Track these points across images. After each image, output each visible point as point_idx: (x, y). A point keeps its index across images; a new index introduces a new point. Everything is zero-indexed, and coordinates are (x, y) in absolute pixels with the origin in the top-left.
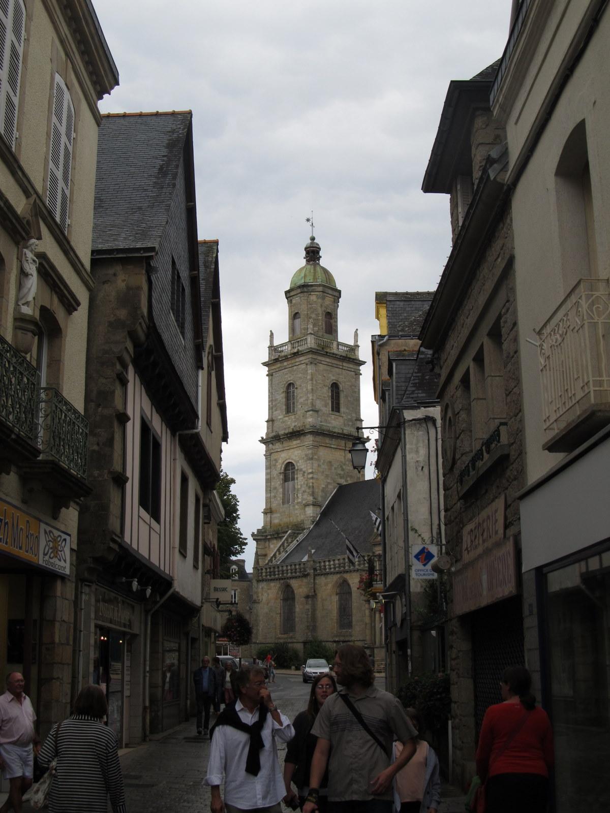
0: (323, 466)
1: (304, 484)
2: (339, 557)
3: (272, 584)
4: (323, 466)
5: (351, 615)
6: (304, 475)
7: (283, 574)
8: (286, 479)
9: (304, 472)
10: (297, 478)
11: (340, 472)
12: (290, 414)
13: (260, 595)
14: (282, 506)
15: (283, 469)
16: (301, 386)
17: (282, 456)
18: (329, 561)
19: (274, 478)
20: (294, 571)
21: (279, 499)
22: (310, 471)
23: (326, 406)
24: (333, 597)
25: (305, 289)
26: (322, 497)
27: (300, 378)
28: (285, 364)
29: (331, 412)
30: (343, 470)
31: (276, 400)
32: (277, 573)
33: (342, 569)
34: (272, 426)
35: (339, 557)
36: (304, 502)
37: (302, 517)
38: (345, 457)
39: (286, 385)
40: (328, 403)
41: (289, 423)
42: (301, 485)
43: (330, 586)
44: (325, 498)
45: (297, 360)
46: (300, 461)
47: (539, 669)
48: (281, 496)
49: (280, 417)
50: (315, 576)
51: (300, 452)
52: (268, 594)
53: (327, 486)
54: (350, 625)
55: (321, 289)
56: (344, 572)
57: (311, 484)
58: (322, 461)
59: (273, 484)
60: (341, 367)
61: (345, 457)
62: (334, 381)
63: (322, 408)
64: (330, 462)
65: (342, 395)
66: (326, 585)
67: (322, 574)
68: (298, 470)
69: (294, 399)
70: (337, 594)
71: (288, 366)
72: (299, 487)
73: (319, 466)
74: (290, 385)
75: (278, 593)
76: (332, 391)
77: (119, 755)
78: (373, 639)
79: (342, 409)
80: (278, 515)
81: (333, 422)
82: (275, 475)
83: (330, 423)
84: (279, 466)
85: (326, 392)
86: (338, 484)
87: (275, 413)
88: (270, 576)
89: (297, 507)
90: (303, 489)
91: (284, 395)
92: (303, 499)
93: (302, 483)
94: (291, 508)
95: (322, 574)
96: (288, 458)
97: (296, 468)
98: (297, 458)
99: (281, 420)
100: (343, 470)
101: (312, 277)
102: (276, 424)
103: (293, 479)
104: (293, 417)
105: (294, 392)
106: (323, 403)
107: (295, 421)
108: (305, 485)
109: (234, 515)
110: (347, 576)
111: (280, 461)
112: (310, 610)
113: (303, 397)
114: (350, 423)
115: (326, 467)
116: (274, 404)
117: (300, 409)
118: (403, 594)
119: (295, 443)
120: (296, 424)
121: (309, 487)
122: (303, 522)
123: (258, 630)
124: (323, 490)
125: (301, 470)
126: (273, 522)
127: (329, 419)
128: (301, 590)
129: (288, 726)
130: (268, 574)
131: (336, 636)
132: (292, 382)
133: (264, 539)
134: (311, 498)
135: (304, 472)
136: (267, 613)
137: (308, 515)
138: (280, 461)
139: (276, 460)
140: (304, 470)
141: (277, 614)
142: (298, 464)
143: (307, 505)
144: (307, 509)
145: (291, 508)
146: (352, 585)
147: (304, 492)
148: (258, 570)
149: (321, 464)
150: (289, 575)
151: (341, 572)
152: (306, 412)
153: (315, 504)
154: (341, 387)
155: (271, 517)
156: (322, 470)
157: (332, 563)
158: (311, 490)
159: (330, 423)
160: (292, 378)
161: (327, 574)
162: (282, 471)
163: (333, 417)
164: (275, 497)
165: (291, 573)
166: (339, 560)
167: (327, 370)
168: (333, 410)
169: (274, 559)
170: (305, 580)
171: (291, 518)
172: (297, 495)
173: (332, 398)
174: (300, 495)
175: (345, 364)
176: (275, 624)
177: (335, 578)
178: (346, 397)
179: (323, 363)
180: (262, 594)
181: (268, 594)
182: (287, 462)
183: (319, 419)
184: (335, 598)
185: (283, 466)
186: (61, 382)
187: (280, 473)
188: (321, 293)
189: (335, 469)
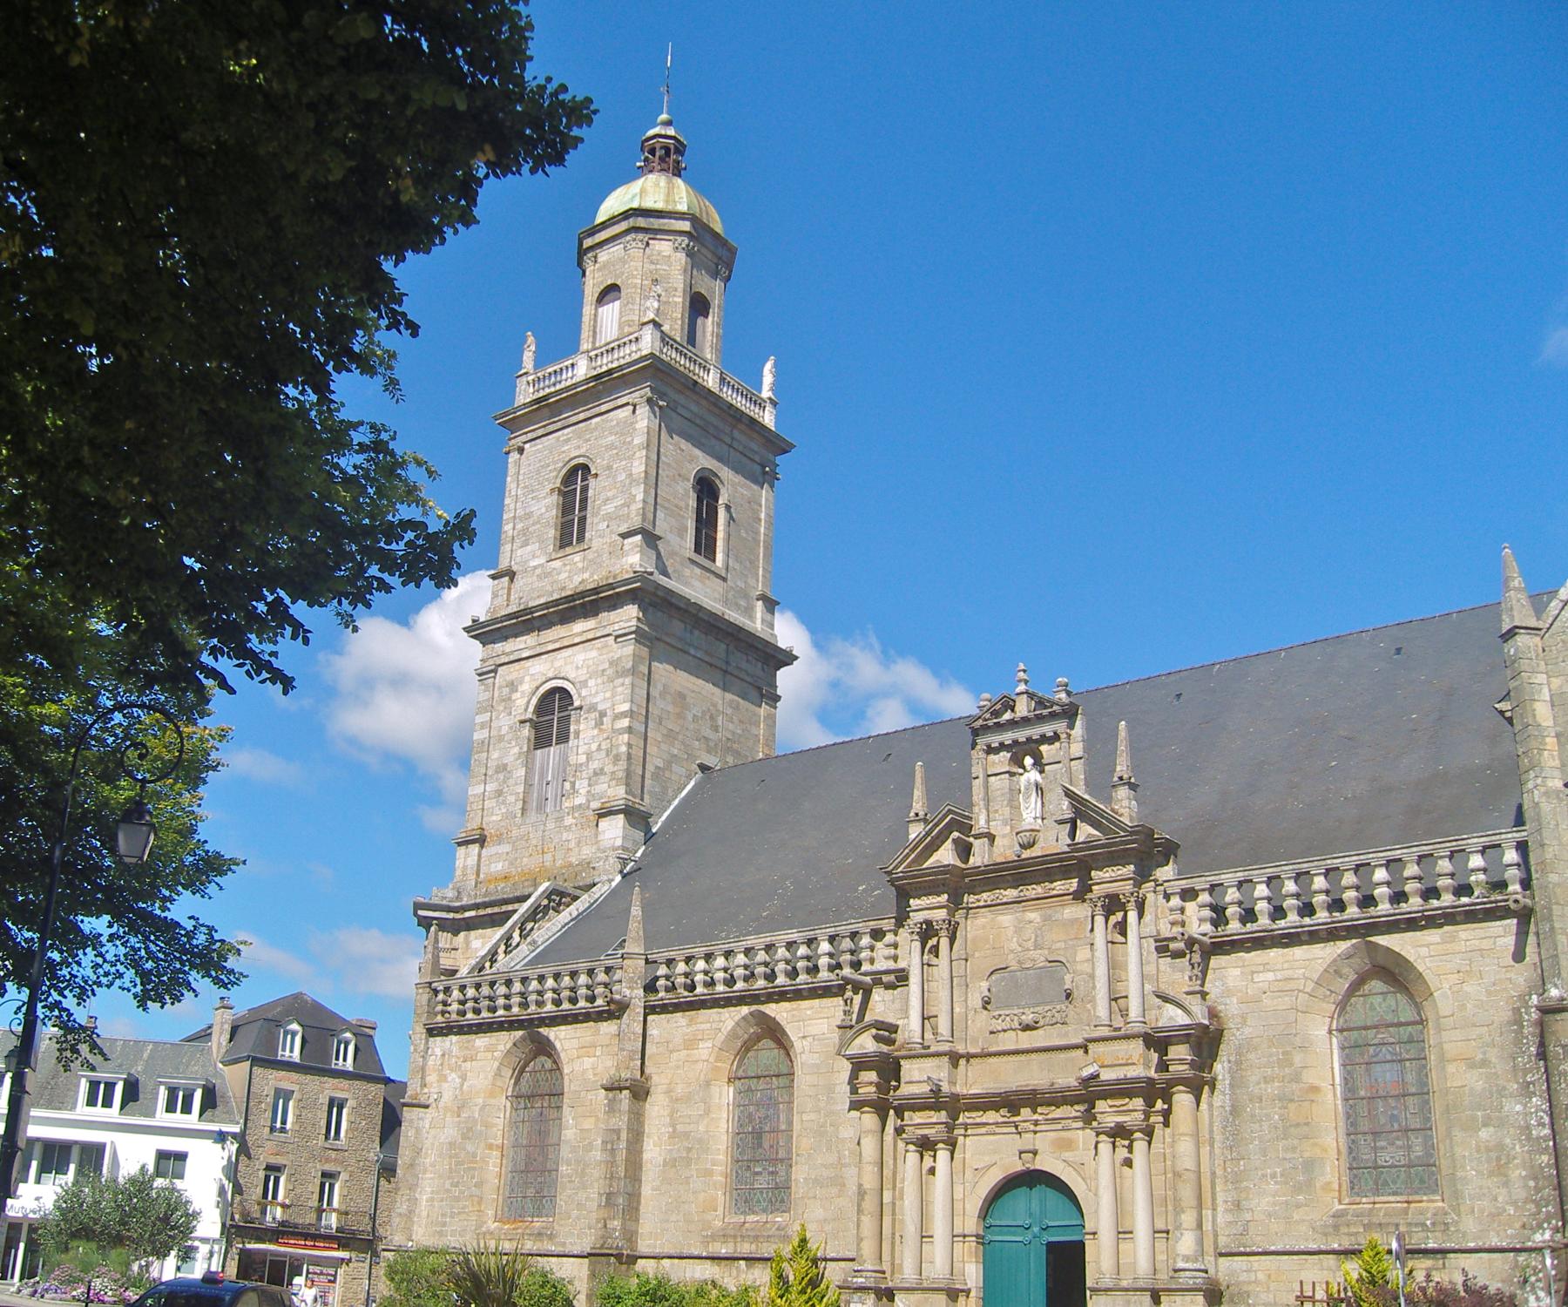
1: (599, 749)
2: (751, 941)
3: (481, 1041)
5: (788, 1162)
7: (524, 1005)
8: (542, 739)
9: (603, 714)
10: (577, 734)
12: (568, 550)
13: (432, 1078)
14: (518, 820)
15: (531, 708)
16: (609, 468)
17: (532, 671)
18: (708, 957)
19: (501, 738)
20: (566, 994)
21: (511, 799)
22: (626, 707)
24: (715, 1090)
25: (641, 222)
27: (611, 447)
30: (716, 729)
31: (529, 515)
32: (501, 1001)
33: (761, 983)
34: (509, 589)
35: (751, 941)
36: (595, 805)
37: (587, 852)
39: (564, 471)
41: (564, 576)
42: (589, 756)
43: (705, 1050)
46: (591, 683)
48: (521, 789)
49: (533, 563)
50: (650, 1010)
51: (594, 654)
52: (464, 1078)
54: (1424, 1175)
57: (624, 749)
59: (495, 755)
60: (728, 440)
64: (682, 696)
66: (690, 1043)
68: (580, 708)
69: (583, 507)
72: (583, 759)
74: (578, 473)
75: (498, 1074)
80: (506, 848)
82: (505, 730)
83: (686, 584)
84: (521, 702)
87: (519, 552)
88: (477, 1011)
89: (569, 821)
90: (595, 765)
91: (555, 499)
92: (591, 796)
93: (594, 747)
94: (551, 825)
96: (550, 675)
97: (577, 704)
98: (582, 674)
99: (538, 571)
100: (716, 729)
101: (662, 197)
102: (519, 582)
103: (564, 738)
104: (577, 558)
105: (585, 489)
107: (583, 570)
108: (603, 754)
109: (349, 462)
111: (526, 687)
112: (624, 1135)
113: (616, 500)
114: (743, 603)
115: (670, 708)
116: (519, 526)
117: (600, 530)
120: (586, 576)
121: (617, 758)
122: (588, 865)
123: (414, 1201)
125: (593, 708)
126: (483, 869)
127: (687, 572)
128: (588, 1062)
130: (470, 1004)
131: (725, 1237)
132: (581, 460)
134: (621, 791)
135: (603, 714)
136: (452, 1145)
137: (606, 844)
139: (513, 686)
140: (600, 707)
141: (490, 1147)
142: (584, 692)
143: (604, 813)
144: (604, 823)
145: (551, 825)
146: (798, 1045)
147: (599, 773)
148: (436, 992)
150: (549, 1007)
152: (625, 536)
153: (636, 817)
155: (479, 855)
157: (720, 962)
158: (623, 765)
160: (582, 451)
161: (702, 1004)
162: (529, 715)
164: (499, 793)
165: (557, 1003)
166: (748, 951)
168: (697, 550)
169: (488, 964)
170: (608, 1027)
171: (548, 857)
172: (573, 784)
174: (582, 786)
175: (736, 434)
176: (479, 1185)
177: (730, 1018)
180: (443, 1078)
181: (464, 1078)
184: (725, 1095)
185: (534, 701)
187: (522, 722)
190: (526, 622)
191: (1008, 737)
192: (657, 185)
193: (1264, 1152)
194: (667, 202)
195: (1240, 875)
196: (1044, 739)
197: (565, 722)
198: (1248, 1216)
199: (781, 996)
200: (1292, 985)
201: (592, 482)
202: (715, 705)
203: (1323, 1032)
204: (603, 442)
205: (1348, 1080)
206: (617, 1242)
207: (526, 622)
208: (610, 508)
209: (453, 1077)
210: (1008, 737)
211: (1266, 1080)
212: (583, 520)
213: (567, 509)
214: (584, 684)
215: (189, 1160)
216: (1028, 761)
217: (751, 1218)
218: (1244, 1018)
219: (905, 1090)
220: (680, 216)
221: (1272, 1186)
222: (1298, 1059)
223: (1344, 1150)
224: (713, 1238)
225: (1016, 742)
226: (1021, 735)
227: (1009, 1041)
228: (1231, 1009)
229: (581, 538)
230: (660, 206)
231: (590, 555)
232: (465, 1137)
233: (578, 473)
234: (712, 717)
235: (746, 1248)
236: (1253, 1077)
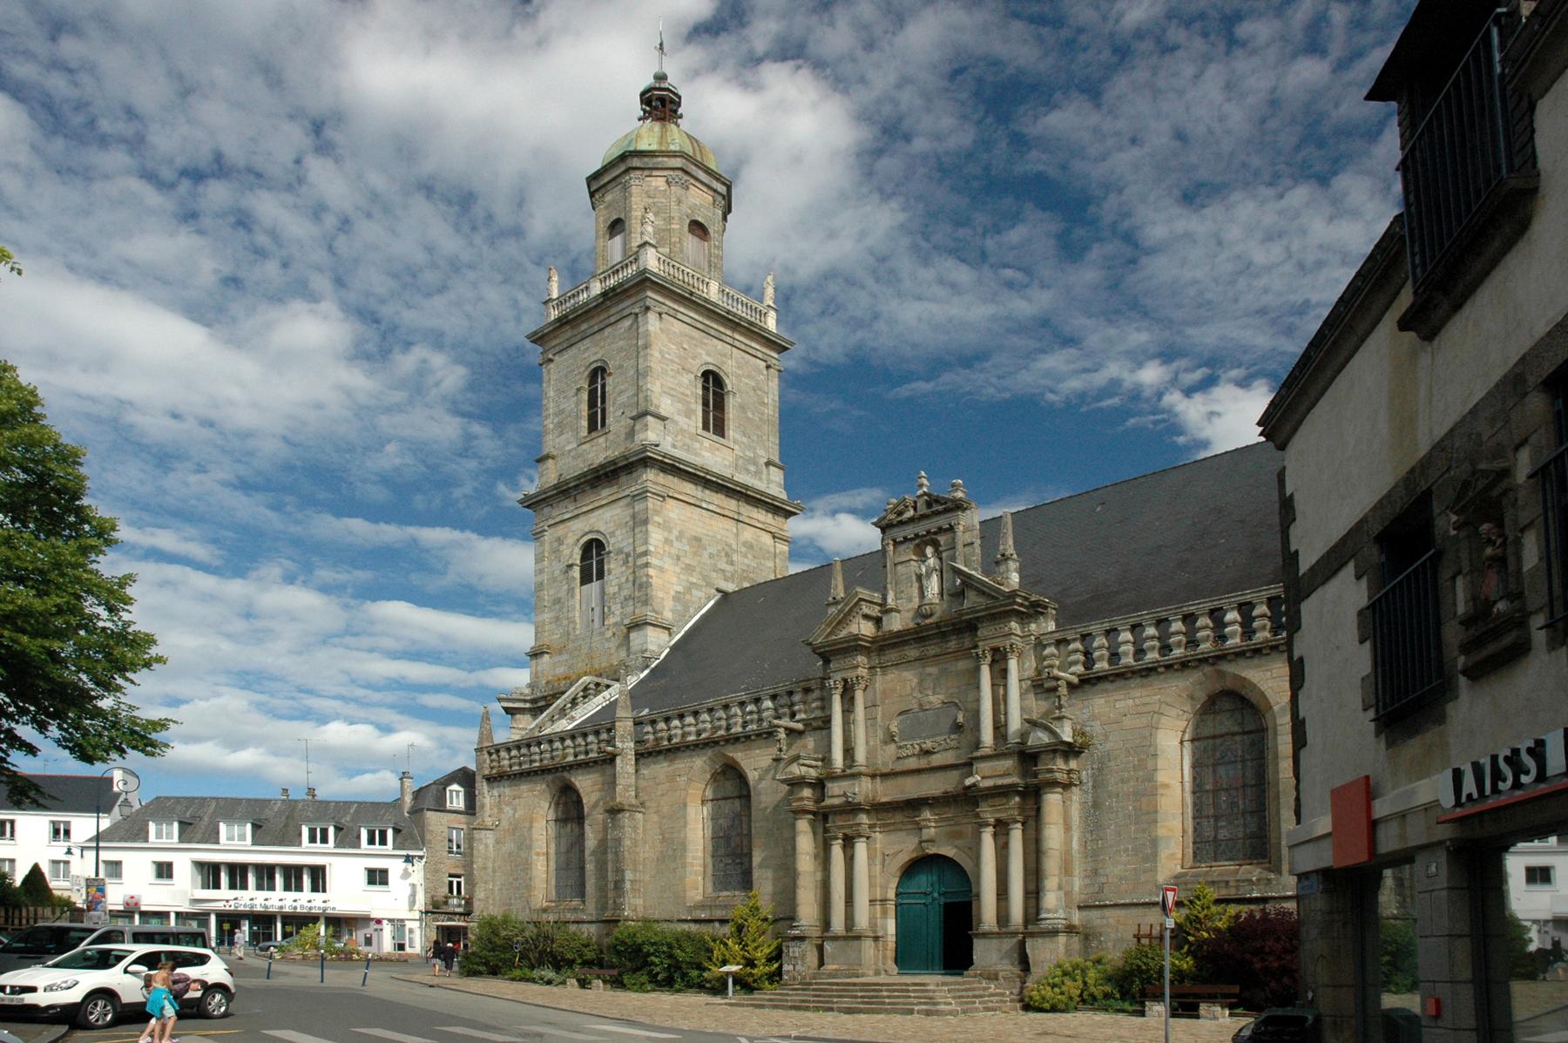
0: (676, 544)
4: (676, 544)
6: (626, 562)
11: (723, 565)
12: (594, 434)
16: (621, 366)
23: (688, 417)
26: (673, 611)
27: (621, 350)
28: (584, 326)
29: (700, 431)
30: (732, 563)
36: (627, 622)
38: (737, 535)
40: (694, 412)
44: (683, 617)
45: (613, 311)
46: (618, 533)
47: (1472, 1023)
51: (618, 511)
53: (688, 590)
55: (678, 162)
56: (727, 741)
58: (675, 533)
61: (737, 535)
62: (711, 368)
63: (677, 418)
65: (731, 404)
67: (660, 752)
70: (703, 802)
71: (590, 332)
73: (667, 541)
76: (705, 389)
77: (1070, 740)
78: (389, 697)
79: (732, 431)
80: (565, 657)
81: (706, 454)
83: (697, 454)
85: (694, 390)
86: (718, 590)
90: (626, 592)
95: (660, 752)
100: (732, 563)
103: (601, 576)
104: (601, 440)
105: (603, 386)
106: (680, 406)
107: (606, 449)
110: (739, 755)
111: (570, 540)
114: (752, 468)
115: (687, 548)
118: (655, 925)
119: (606, 493)
124: (677, 597)
127: (697, 445)
129: (1280, 213)
133: (530, 710)
138: (570, 540)
149: (673, 537)
151: (716, 743)
154: (729, 384)
156: (673, 551)
159: (697, 454)
160: (599, 356)
163: (707, 443)
167: (693, 338)
168: (706, 427)
173: (705, 404)
174: (617, 609)
178: (742, 408)
179: (680, 316)
181: (515, 810)
182: (586, 539)
183: (669, 439)
186: (709, 860)
188: (680, 173)
189: (711, 556)
190: (565, 491)
191: (909, 531)
192: (651, 130)
193: (1119, 834)
194: (661, 144)
195: (1107, 626)
196: (940, 530)
197: (601, 564)
198: (1103, 880)
199: (735, 740)
200: (1149, 708)
201: (609, 380)
202: (729, 546)
203: (1176, 743)
204: (615, 346)
205: (1197, 780)
206: (608, 915)
207: (565, 491)
208: (623, 399)
209: (507, 809)
210: (909, 531)
211: (1122, 781)
212: (604, 410)
213: (592, 404)
214: (612, 534)
215: (124, 865)
216: (929, 551)
217: (725, 893)
218: (1106, 736)
219: (828, 802)
220: (674, 154)
221: (1124, 858)
222: (1150, 764)
223: (1190, 831)
224: (696, 907)
225: (917, 536)
226: (921, 528)
227: (912, 763)
228: (1096, 728)
229: (603, 424)
230: (654, 147)
231: (611, 437)
232: (520, 848)
233: (598, 373)
234: (727, 555)
235: (719, 914)
236: (1112, 780)
